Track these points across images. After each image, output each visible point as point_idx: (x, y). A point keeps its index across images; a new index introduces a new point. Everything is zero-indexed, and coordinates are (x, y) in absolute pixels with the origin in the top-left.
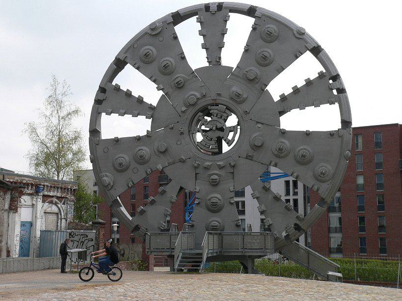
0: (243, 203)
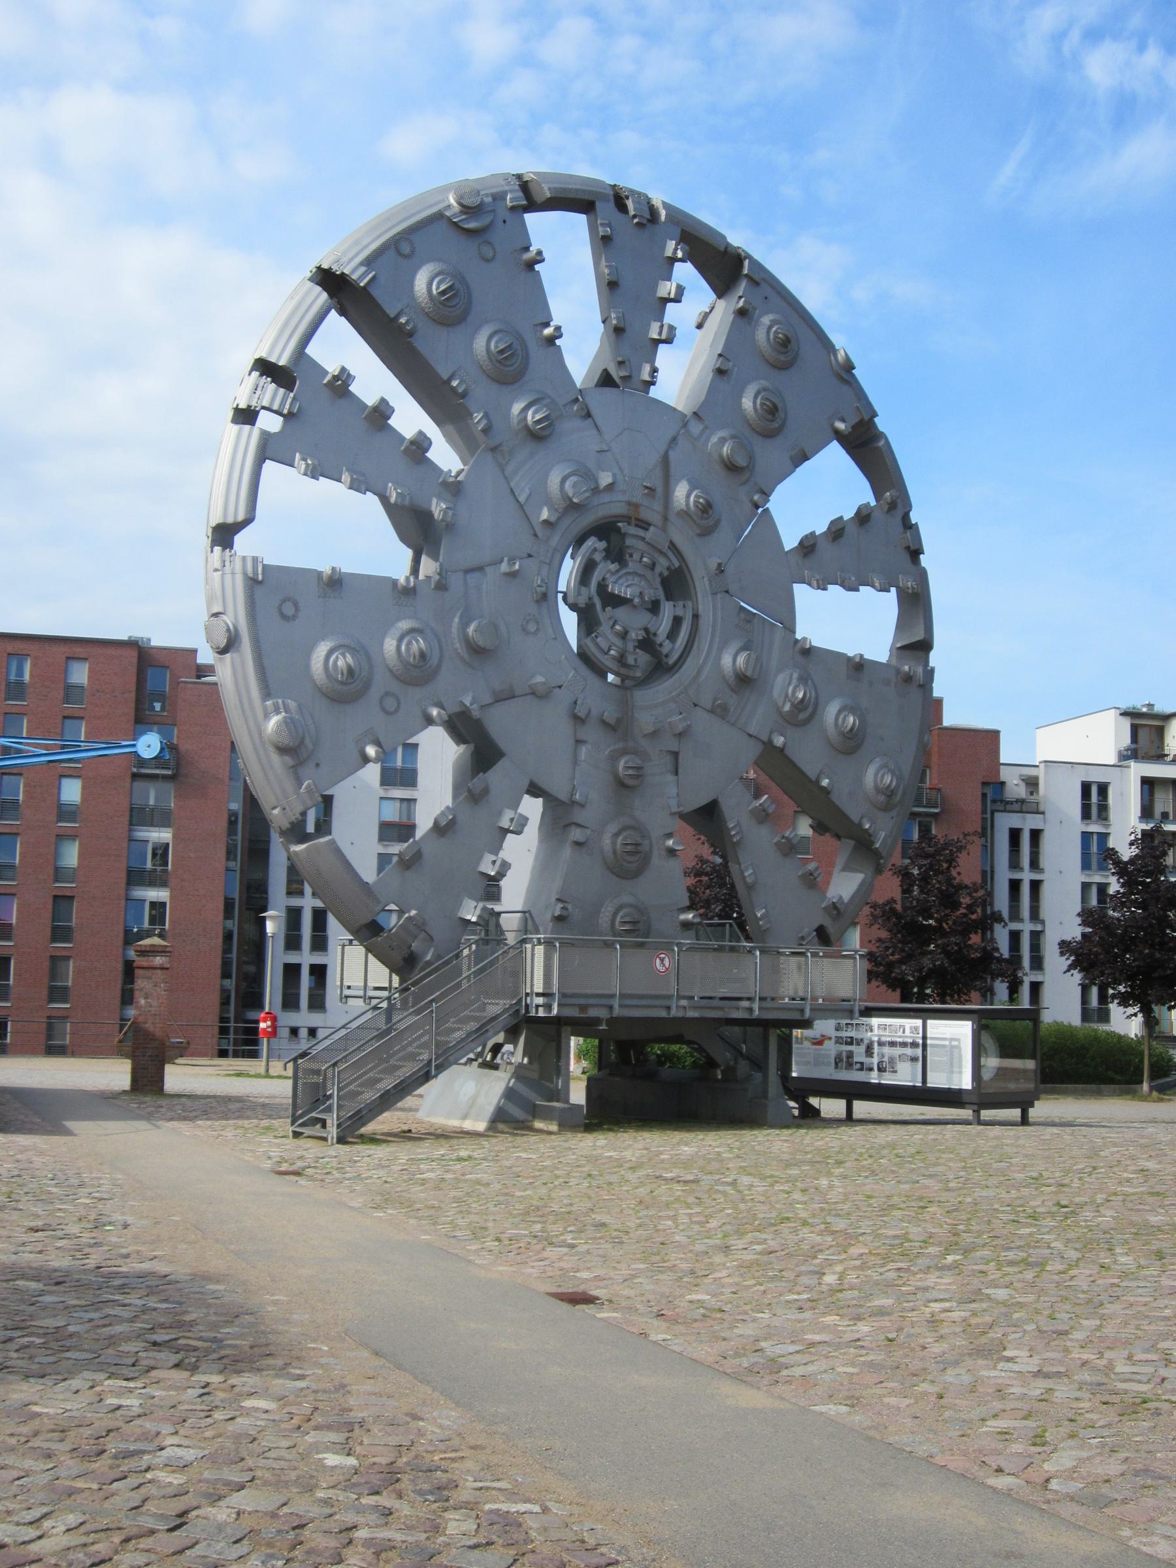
0: (1036, 835)
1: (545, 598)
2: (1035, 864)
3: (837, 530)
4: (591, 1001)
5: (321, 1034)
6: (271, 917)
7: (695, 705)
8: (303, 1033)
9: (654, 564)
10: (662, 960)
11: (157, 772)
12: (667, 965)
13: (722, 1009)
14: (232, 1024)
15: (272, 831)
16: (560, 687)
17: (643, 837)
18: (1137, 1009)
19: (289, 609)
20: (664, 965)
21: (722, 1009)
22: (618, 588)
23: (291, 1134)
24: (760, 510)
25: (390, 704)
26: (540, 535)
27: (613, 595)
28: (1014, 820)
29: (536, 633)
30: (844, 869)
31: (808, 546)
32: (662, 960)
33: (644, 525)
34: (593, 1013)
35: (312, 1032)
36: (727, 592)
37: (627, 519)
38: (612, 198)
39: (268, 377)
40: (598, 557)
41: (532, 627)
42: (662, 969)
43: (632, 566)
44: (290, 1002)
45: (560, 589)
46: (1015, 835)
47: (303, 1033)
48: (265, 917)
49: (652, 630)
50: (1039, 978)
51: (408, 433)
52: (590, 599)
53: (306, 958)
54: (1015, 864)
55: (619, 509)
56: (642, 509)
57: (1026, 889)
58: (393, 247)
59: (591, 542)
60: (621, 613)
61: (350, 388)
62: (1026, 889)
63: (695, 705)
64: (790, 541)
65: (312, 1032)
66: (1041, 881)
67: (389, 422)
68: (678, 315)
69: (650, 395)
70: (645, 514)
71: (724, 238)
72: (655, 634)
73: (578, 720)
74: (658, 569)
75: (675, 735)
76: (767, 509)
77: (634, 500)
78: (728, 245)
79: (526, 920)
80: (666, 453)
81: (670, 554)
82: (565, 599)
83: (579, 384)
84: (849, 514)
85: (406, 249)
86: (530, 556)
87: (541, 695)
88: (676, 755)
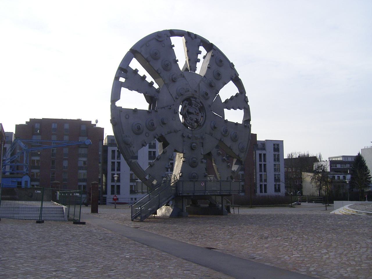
0: (265, 155)
1: (176, 113)
2: (265, 161)
3: (232, 98)
4: (190, 192)
5: (137, 199)
6: (116, 176)
7: (206, 133)
8: (134, 199)
9: (197, 106)
10: (203, 184)
11: (84, 146)
14: (101, 198)
15: (284, 181)
16: (180, 130)
17: (197, 159)
18: (323, 193)
19: (127, 117)
22: (191, 110)
23: (131, 220)
24: (217, 95)
25: (147, 134)
26: (175, 100)
27: (190, 112)
28: (258, 152)
30: (235, 164)
31: (227, 101)
32: (203, 184)
33: (196, 98)
34: (190, 194)
35: (135, 199)
37: (192, 97)
38: (187, 34)
40: (186, 105)
41: (174, 119)
43: (193, 106)
44: (113, 193)
45: (179, 111)
46: (260, 155)
47: (134, 199)
48: (114, 177)
49: (197, 119)
50: (266, 184)
51: (149, 82)
52: (185, 113)
54: (260, 161)
55: (191, 95)
58: (145, 45)
59: (186, 102)
60: (191, 116)
61: (138, 73)
64: (223, 101)
65: (135, 199)
66: (266, 164)
67: (146, 79)
68: (200, 57)
69: (196, 72)
70: (195, 96)
71: (209, 41)
72: (198, 120)
73: (183, 137)
74: (198, 107)
76: (219, 95)
78: (210, 43)
79: (174, 176)
81: (200, 104)
82: (180, 114)
83: (181, 70)
85: (148, 45)
86: (173, 105)
87: (176, 132)
88: (202, 143)
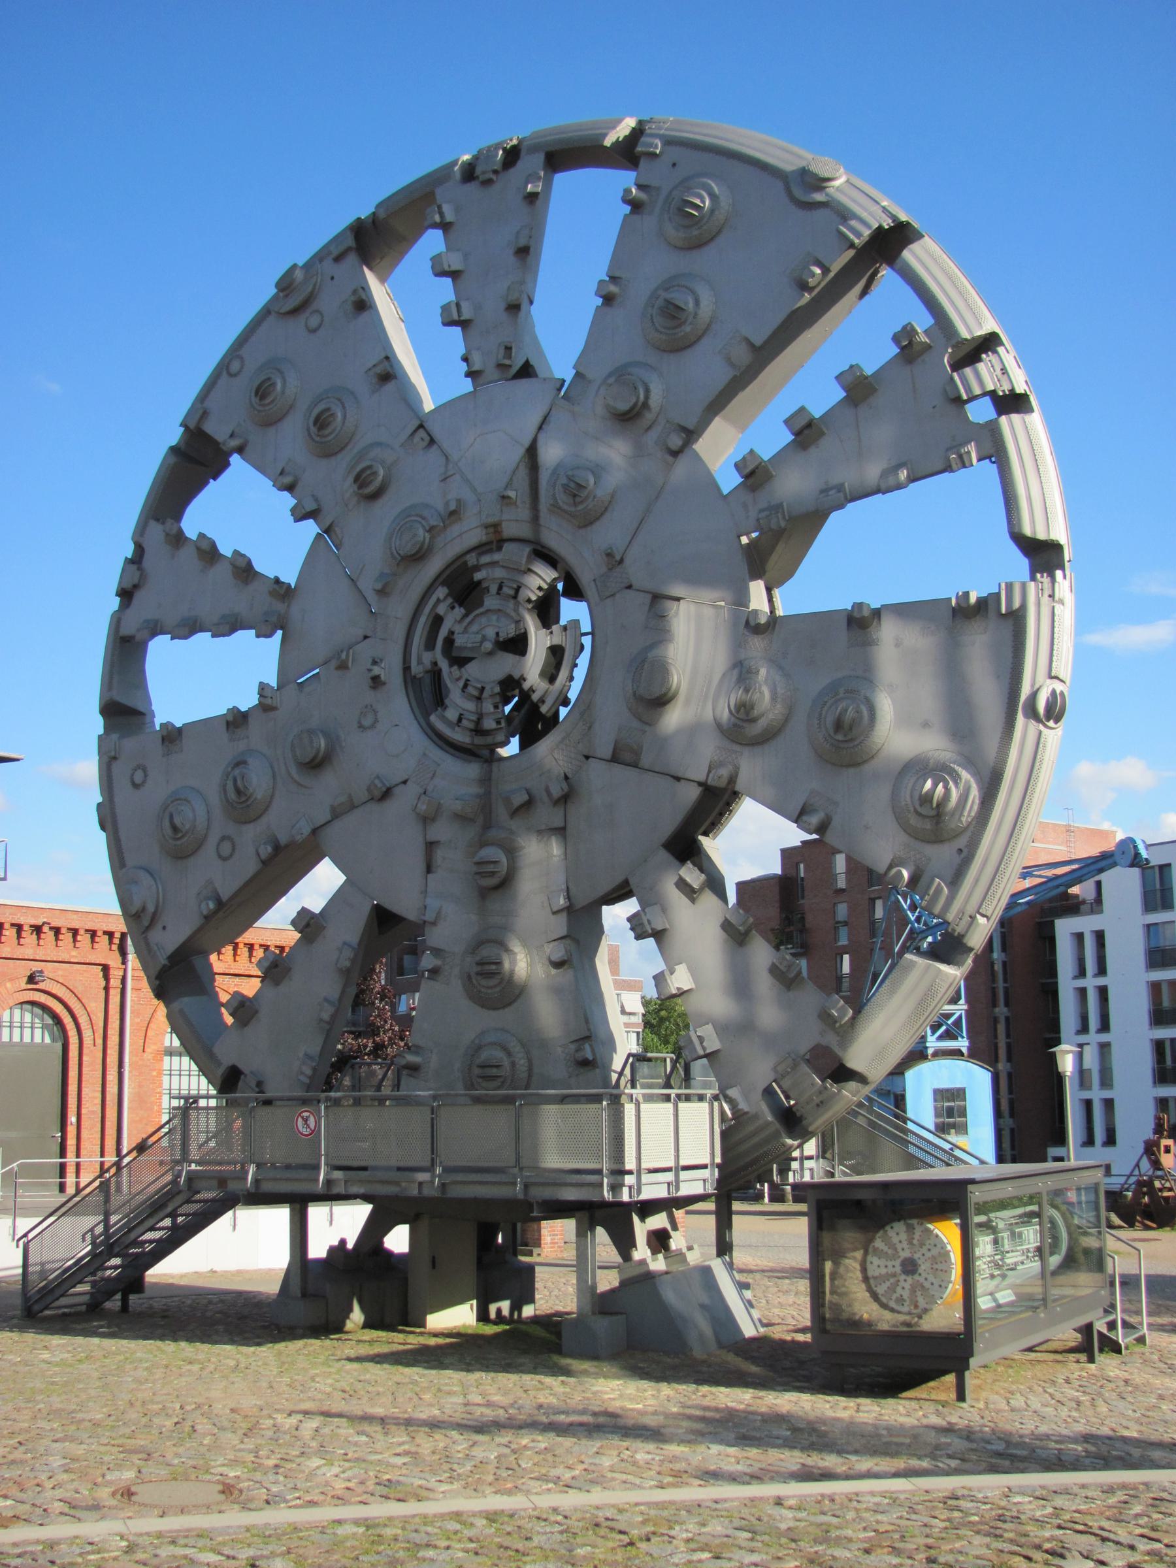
7: (587, 757)
10: (306, 1120)
12: (312, 1126)
13: (397, 1183)
16: (405, 782)
20: (308, 1126)
21: (397, 1183)
29: (373, 726)
32: (306, 1120)
36: (629, 587)
39: (1005, 396)
40: (441, 610)
42: (306, 1131)
53: (1097, 1095)
56: (504, 525)
57: (1090, 965)
62: (1090, 965)
63: (587, 757)
75: (556, 803)
77: (491, 520)
80: (534, 442)
84: (287, 500)
86: (366, 637)
